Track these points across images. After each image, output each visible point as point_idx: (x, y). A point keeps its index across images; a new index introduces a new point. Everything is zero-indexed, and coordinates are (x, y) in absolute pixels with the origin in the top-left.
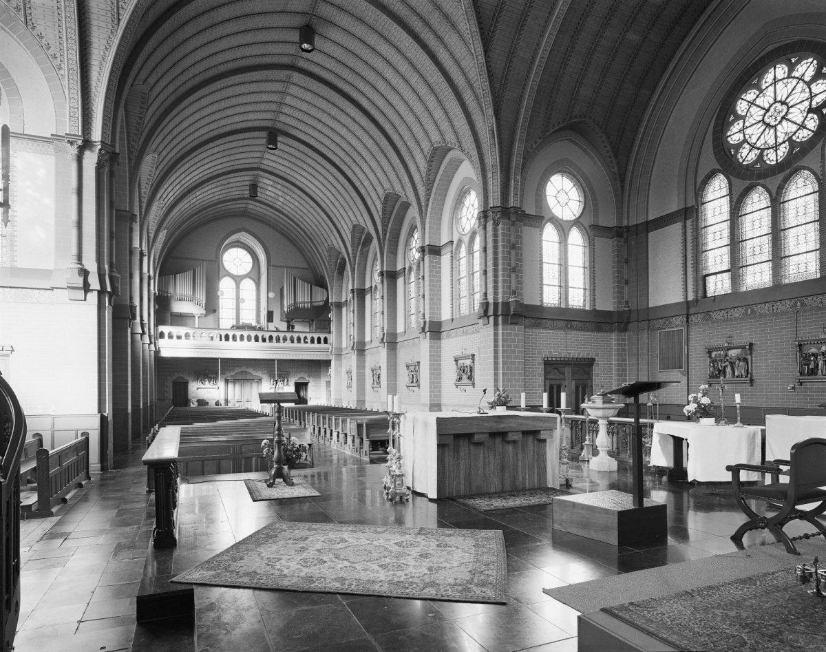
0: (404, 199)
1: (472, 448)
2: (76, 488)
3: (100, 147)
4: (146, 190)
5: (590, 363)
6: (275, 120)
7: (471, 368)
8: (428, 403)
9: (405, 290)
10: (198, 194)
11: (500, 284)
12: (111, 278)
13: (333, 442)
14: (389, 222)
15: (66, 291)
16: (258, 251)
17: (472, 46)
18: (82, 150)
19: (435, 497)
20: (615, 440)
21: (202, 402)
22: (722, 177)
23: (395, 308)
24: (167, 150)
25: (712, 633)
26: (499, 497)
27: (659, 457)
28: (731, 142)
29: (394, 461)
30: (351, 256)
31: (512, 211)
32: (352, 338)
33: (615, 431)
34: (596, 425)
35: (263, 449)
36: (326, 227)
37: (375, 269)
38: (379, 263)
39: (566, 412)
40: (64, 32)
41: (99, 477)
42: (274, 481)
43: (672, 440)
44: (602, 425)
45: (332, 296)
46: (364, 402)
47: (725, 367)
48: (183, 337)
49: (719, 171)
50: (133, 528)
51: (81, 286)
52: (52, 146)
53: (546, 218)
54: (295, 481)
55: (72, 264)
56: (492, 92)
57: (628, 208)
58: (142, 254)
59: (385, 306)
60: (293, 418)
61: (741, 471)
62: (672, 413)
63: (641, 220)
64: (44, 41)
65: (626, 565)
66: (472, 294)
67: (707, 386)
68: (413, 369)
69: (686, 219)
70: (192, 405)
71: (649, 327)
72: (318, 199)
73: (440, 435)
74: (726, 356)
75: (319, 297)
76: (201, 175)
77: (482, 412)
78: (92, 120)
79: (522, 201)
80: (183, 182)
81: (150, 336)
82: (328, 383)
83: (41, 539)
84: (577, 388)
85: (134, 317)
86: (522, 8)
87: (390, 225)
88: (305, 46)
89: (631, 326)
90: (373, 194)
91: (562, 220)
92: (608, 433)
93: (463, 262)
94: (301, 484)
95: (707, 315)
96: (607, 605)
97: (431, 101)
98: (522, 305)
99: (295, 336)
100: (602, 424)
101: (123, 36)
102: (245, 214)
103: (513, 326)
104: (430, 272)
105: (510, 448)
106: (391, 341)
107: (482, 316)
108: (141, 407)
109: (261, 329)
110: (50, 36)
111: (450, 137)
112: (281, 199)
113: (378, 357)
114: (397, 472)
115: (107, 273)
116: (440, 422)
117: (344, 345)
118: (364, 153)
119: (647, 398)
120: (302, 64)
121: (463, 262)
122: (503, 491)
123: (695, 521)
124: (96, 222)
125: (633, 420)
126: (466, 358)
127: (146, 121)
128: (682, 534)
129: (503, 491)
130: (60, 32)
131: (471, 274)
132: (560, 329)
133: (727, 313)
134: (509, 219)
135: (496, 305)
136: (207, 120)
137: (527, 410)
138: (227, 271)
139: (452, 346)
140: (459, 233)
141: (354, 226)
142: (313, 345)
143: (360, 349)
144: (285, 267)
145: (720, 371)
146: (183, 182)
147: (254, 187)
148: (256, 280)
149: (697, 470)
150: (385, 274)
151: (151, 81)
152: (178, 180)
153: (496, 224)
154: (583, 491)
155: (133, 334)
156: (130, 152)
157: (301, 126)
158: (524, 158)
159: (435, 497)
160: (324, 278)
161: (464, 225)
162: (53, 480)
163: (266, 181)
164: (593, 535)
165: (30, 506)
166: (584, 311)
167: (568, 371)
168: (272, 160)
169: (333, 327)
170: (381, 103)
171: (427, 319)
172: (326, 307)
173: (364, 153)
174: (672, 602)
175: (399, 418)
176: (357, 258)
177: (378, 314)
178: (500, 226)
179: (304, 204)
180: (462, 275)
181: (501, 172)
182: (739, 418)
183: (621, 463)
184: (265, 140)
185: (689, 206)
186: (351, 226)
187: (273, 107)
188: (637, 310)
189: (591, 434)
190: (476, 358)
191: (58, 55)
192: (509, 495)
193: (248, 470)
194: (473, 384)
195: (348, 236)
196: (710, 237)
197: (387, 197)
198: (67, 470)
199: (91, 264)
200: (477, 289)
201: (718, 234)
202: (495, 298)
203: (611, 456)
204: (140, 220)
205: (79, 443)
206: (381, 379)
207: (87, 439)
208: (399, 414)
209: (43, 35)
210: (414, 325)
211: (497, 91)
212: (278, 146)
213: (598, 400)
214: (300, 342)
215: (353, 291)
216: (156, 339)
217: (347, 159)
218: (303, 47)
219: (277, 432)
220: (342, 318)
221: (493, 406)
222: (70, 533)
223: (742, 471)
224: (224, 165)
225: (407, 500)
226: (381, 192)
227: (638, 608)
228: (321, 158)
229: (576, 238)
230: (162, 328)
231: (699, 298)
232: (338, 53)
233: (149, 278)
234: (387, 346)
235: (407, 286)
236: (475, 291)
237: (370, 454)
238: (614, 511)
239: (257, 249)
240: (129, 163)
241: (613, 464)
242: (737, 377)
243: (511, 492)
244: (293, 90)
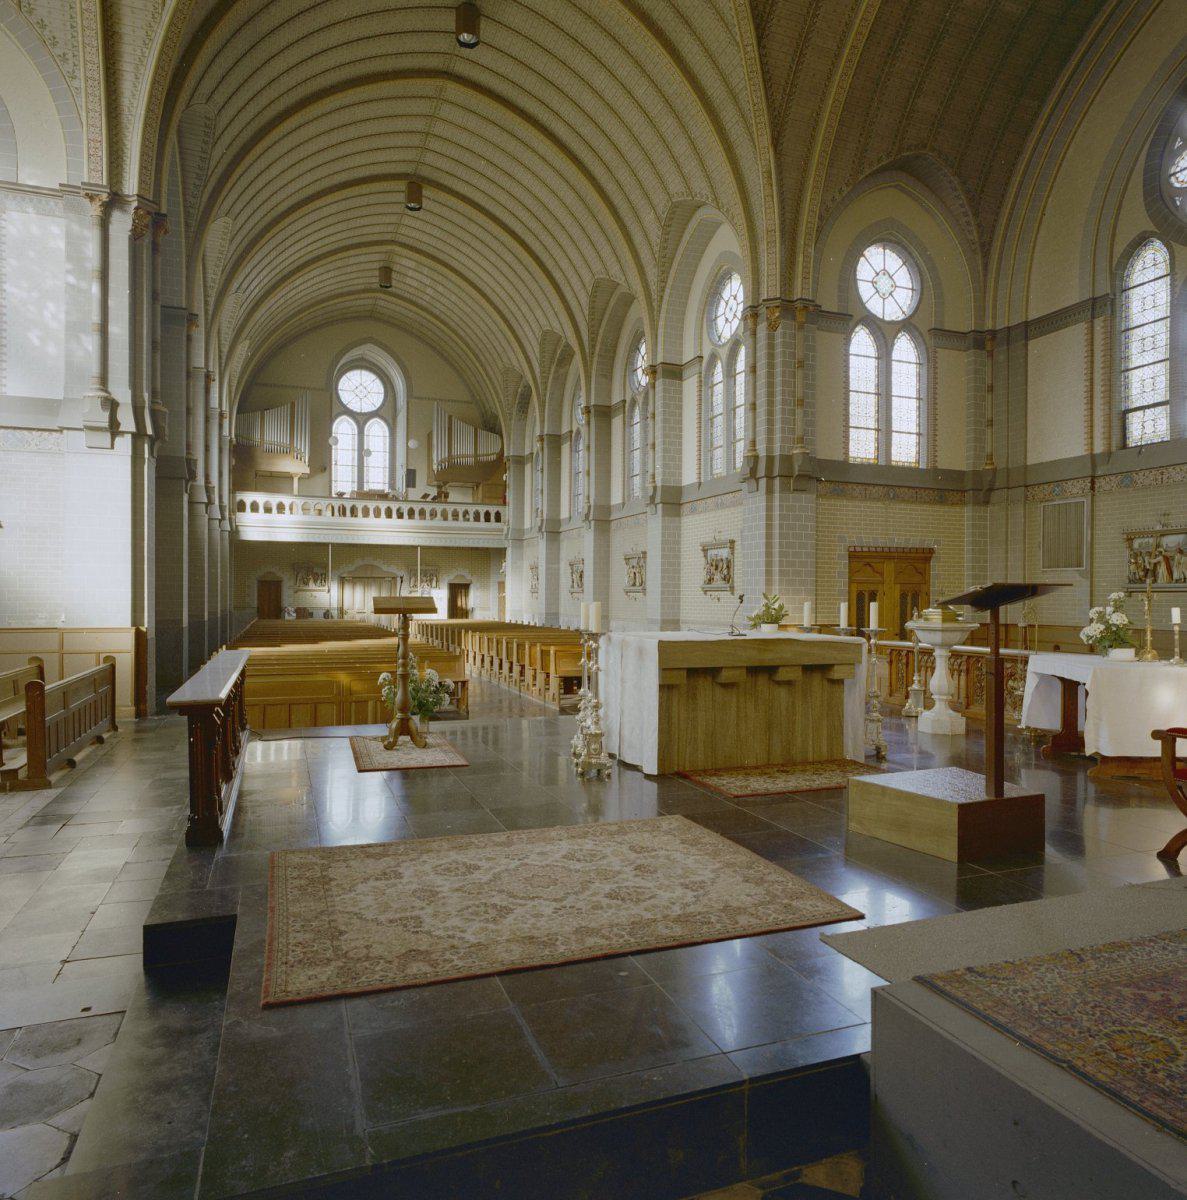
0: (623, 289)
1: (719, 691)
2: (93, 744)
3: (135, 204)
4: (215, 276)
5: (925, 556)
6: (419, 162)
7: (729, 562)
8: (659, 618)
10: (298, 282)
11: (778, 426)
12: (153, 413)
13: (502, 679)
14: (599, 326)
15: (82, 434)
16: (393, 373)
17: (737, 30)
19: (654, 771)
20: (963, 682)
21: (303, 613)
22: (1157, 243)
23: (608, 472)
24: (248, 211)
25: (1114, 1032)
26: (761, 775)
27: (1035, 711)
28: (1177, 185)
29: (589, 712)
30: (539, 381)
31: (798, 305)
32: (539, 513)
33: (964, 667)
34: (932, 658)
35: (382, 686)
36: (499, 335)
37: (576, 403)
38: (583, 393)
39: (879, 635)
40: (79, 17)
41: (132, 727)
42: (396, 738)
43: (1059, 686)
44: (941, 657)
45: (509, 445)
46: (556, 615)
47: (1155, 564)
48: (274, 510)
49: (1153, 234)
50: (172, 810)
51: (106, 425)
52: (61, 203)
53: (856, 318)
54: (430, 740)
55: (93, 392)
56: (769, 107)
57: (995, 300)
58: (208, 377)
59: (593, 462)
60: (432, 637)
61: (1178, 739)
62: (1061, 641)
63: (1017, 320)
64: (46, 32)
65: (971, 897)
66: (731, 442)
67: (1122, 594)
69: (1093, 317)
70: (287, 617)
71: (1026, 497)
72: (488, 292)
73: (664, 669)
74: (1158, 546)
75: (489, 448)
76: (302, 252)
77: (737, 632)
78: (123, 161)
79: (815, 291)
80: (275, 263)
81: (222, 508)
82: (501, 585)
83: (27, 825)
84: (903, 596)
85: (192, 475)
87: (601, 331)
88: (466, 37)
89: (995, 496)
90: (574, 280)
91: (883, 320)
92: (952, 671)
93: (719, 389)
94: (439, 745)
95: (1127, 477)
96: (921, 972)
97: (668, 124)
99: (450, 509)
100: (941, 656)
101: (172, 24)
102: (372, 316)
103: (796, 495)
104: (665, 405)
105: (782, 693)
106: (602, 519)
107: (748, 479)
108: (206, 618)
109: (395, 499)
111: (699, 185)
112: (429, 290)
113: (581, 544)
114: (593, 730)
115: (147, 405)
116: (663, 646)
117: (527, 525)
119: (1013, 613)
120: (461, 68)
121: (719, 389)
122: (769, 765)
123: (1098, 821)
124: (130, 324)
125: (988, 650)
126: (718, 546)
127: (213, 163)
128: (1073, 843)
129: (769, 765)
130: (72, 17)
131: (731, 410)
132: (878, 500)
133: (1162, 474)
134: (794, 318)
135: (770, 459)
136: (309, 164)
137: (846, 634)
138: (344, 406)
139: (698, 528)
140: (713, 344)
141: (545, 333)
142: (477, 524)
143: (553, 531)
144: (436, 400)
145: (1146, 571)
146: (275, 263)
147: (386, 272)
148: (390, 421)
149: (1101, 738)
150: (592, 411)
151: (219, 98)
152: (266, 261)
153: (772, 327)
154: (905, 766)
155: (191, 503)
156: (187, 214)
157: (460, 171)
158: (821, 218)
159: (654, 771)
160: (497, 417)
161: (720, 329)
162: (53, 730)
163: (404, 261)
164: (919, 844)
165: (15, 772)
166: (917, 470)
167: (889, 568)
168: (414, 227)
170: (586, 129)
171: (659, 484)
172: (498, 464)
174: (1043, 969)
175: (596, 641)
176: (549, 385)
177: (580, 475)
178: (780, 330)
179: (466, 298)
180: (716, 412)
181: (783, 242)
182: (1177, 650)
183: (970, 721)
184: (403, 195)
186: (539, 334)
187: (416, 140)
188: (1008, 469)
189: (923, 672)
190: (738, 546)
191: (70, 56)
192: (778, 771)
193: (362, 720)
195: (534, 351)
196: (1135, 347)
197: (596, 286)
198: (77, 717)
199: (122, 392)
200: (740, 433)
201: (1148, 342)
202: (769, 449)
203: (955, 709)
204: (206, 324)
205: (98, 672)
206: (585, 579)
207: (113, 667)
208: (597, 634)
209: (46, 22)
210: (637, 492)
211: (777, 104)
212: (424, 206)
213: (934, 615)
214: (457, 520)
215: (541, 438)
216: (232, 512)
217: (533, 224)
218: (462, 40)
219: (400, 661)
220: (524, 486)
221: (757, 623)
222: (72, 816)
225: (609, 776)
226: (587, 278)
227: (980, 979)
228: (327, 101)
229: (905, 349)
230: (240, 496)
231: (1114, 449)
232: (518, 47)
233: (221, 415)
234: (595, 525)
235: (627, 430)
236: (738, 438)
237: (560, 699)
238: (952, 803)
239: (391, 371)
240: (186, 231)
241: (959, 724)
242: (1177, 581)
243: (782, 765)
244: (446, 111)
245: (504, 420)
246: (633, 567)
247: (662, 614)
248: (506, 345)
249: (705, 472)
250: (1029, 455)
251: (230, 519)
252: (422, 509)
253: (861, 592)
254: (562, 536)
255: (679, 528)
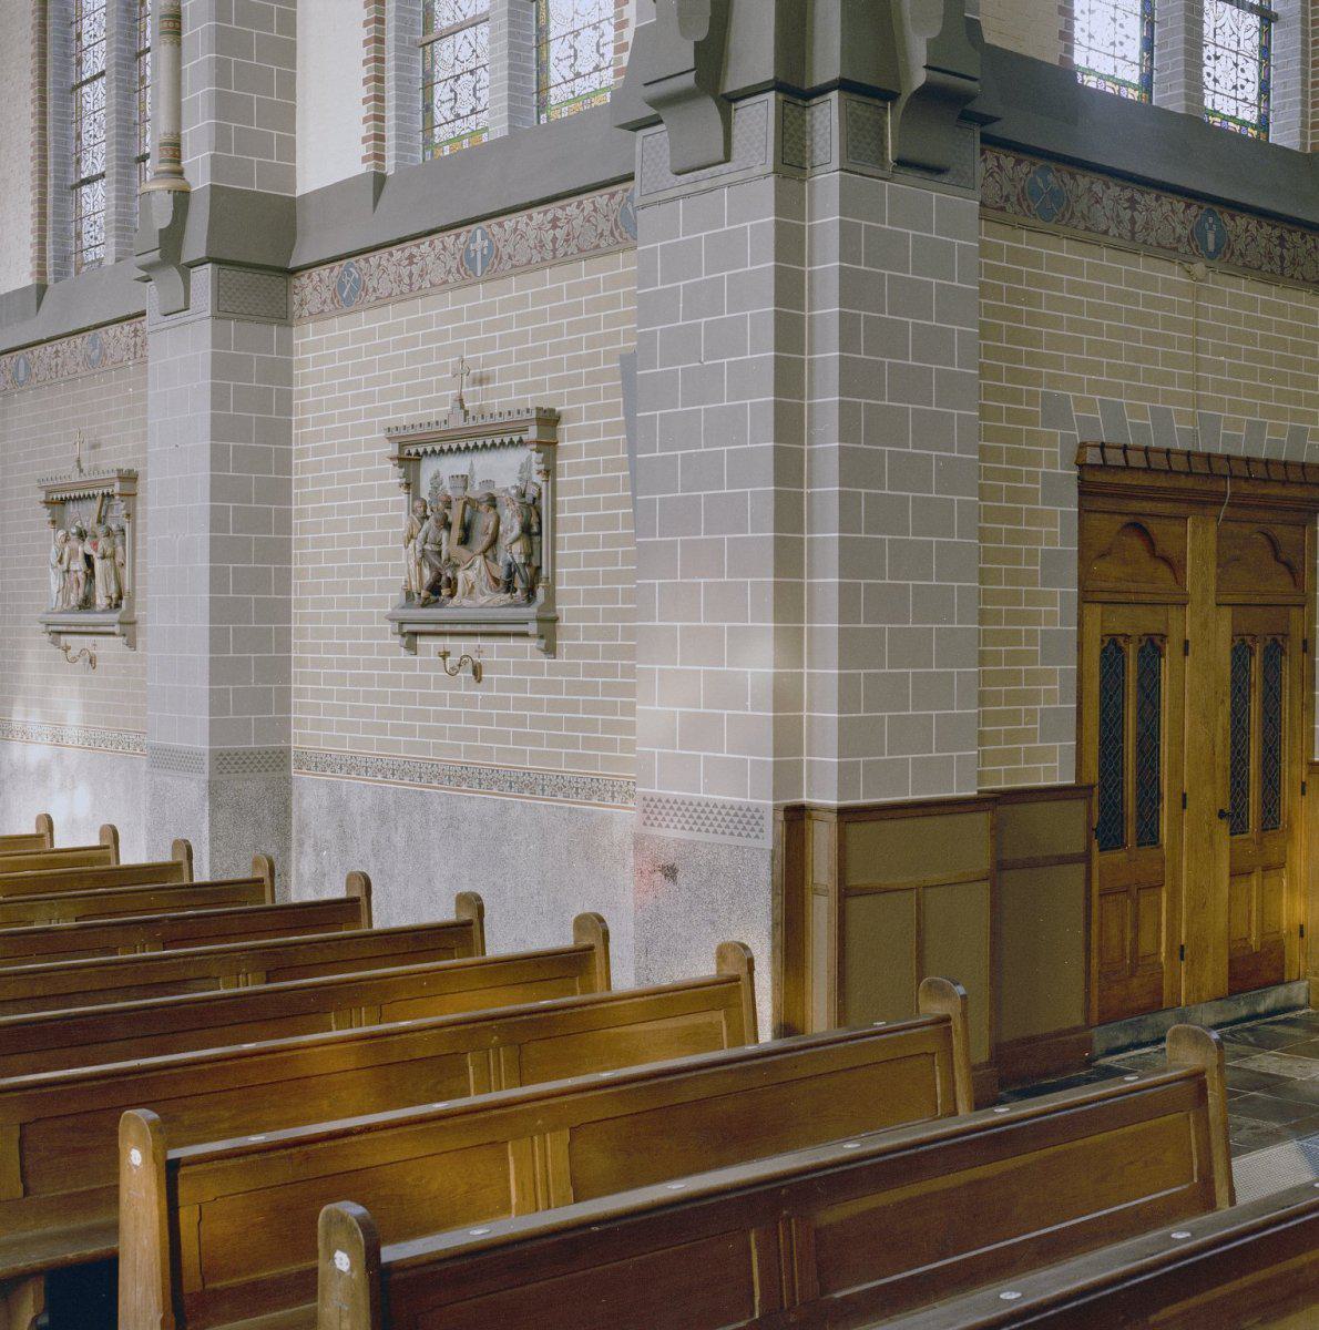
8: (202, 745)
9: (42, 26)
68: (89, 523)
84: (1240, 653)
132: (1166, 251)
171: (199, 177)
194: (548, 630)
246: (82, 535)
247: (215, 730)
249: (403, 135)
253: (1113, 639)
255: (283, 372)
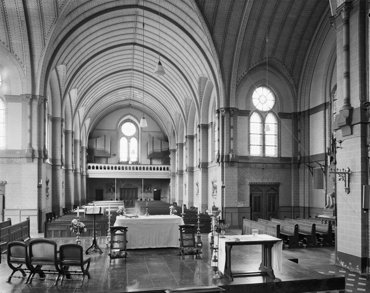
10: (103, 100)
18: (32, 100)
36: (165, 112)
45: (171, 146)
59: (188, 153)
63: (306, 109)
64: (17, 57)
66: (213, 151)
69: (325, 109)
75: (164, 148)
86: (227, 11)
90: (180, 97)
98: (236, 156)
108: (80, 200)
110: (20, 55)
118: (174, 79)
136: (99, 70)
152: (91, 97)
169: (171, 162)
173: (174, 79)
185: (327, 102)
191: (22, 62)
209: (17, 55)
211: (220, 51)
223: (201, 244)
224: (113, 87)
230: (89, 164)
245: (169, 138)
248: (167, 116)
250: (310, 152)
251: (86, 172)
252: (147, 167)
254: (194, 172)
